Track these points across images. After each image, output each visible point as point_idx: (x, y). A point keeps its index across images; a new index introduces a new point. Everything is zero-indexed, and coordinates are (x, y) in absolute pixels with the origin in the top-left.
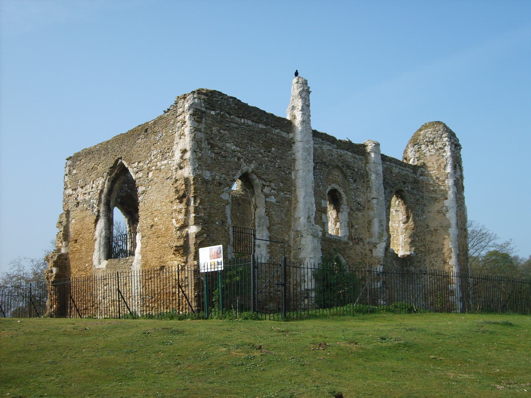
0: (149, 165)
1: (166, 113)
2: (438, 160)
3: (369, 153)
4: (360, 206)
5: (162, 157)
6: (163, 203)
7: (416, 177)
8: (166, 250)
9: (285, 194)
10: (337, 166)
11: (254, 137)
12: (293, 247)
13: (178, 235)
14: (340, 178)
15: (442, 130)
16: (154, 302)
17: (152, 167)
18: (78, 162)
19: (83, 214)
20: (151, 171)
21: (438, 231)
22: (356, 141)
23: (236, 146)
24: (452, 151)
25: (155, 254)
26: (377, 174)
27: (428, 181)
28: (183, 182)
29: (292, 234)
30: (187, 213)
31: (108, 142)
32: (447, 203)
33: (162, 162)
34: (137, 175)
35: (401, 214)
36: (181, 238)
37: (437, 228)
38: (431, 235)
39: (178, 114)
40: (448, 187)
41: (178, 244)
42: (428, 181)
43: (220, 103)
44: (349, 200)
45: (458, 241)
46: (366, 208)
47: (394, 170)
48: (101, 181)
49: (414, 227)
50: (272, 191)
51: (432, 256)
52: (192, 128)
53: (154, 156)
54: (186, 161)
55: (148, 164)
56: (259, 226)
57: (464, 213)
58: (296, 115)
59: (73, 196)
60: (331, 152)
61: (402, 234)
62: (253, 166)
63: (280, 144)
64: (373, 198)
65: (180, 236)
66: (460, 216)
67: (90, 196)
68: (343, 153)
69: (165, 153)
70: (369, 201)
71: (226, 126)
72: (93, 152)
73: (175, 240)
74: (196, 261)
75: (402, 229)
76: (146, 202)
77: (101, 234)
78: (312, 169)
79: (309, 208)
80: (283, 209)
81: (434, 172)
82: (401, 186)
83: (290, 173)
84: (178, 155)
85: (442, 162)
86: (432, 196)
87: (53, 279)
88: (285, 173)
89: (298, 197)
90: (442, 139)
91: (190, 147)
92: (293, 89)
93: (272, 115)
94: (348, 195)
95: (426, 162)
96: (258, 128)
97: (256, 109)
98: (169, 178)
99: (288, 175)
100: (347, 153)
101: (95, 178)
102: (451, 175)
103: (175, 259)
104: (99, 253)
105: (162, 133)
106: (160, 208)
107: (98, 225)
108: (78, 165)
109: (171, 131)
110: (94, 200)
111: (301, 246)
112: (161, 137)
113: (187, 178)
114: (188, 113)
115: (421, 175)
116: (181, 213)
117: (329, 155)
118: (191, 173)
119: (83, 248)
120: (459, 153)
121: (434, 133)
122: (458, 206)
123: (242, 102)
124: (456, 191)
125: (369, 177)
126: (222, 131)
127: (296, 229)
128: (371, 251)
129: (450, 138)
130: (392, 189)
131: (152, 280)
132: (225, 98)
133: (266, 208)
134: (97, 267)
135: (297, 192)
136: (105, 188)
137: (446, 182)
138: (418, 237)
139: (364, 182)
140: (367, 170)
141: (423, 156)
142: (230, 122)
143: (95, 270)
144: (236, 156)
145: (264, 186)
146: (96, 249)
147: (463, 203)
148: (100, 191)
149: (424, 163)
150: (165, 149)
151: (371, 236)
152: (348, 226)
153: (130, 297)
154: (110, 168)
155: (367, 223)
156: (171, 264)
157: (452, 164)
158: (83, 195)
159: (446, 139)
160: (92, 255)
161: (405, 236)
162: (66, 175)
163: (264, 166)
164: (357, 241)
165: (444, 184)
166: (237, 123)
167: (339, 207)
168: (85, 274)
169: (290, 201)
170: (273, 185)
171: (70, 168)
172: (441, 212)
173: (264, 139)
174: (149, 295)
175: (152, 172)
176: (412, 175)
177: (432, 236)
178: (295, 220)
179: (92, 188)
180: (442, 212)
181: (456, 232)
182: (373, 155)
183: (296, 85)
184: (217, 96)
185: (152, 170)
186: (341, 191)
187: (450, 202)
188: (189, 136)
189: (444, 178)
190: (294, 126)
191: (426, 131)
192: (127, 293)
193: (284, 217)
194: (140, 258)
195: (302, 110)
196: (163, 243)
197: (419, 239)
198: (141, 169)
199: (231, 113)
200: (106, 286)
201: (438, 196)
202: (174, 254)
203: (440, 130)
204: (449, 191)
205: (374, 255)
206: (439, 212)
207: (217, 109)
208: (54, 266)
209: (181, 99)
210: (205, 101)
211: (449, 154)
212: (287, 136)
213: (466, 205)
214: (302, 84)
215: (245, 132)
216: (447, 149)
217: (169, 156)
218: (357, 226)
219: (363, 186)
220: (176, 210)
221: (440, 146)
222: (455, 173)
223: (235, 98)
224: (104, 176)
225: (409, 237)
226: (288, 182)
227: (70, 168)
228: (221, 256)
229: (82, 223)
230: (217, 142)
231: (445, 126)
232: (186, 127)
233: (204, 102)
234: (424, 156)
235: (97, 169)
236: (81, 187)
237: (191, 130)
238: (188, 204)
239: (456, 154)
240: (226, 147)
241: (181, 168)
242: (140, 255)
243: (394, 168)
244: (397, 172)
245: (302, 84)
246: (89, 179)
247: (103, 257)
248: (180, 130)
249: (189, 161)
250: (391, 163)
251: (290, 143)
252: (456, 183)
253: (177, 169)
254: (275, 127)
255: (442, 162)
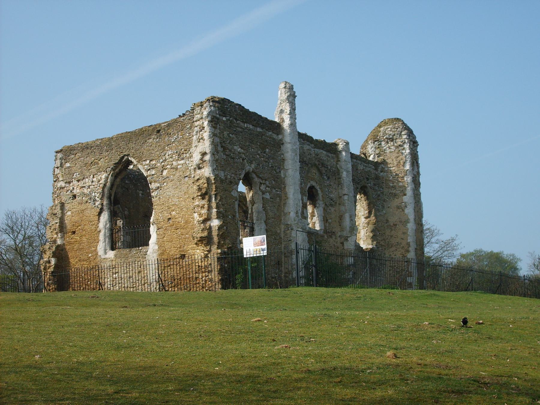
0: (163, 164)
1: (182, 117)
2: (398, 157)
3: (340, 152)
4: (333, 201)
5: (178, 157)
6: (181, 199)
7: (377, 173)
8: (187, 240)
9: (276, 191)
10: (315, 165)
11: (254, 139)
12: (283, 239)
13: (202, 227)
14: (317, 176)
15: (401, 127)
16: (175, 286)
17: (167, 166)
18: (73, 156)
19: (83, 207)
20: (166, 169)
21: (398, 226)
22: (329, 140)
23: (241, 148)
24: (411, 149)
25: (174, 244)
26: (348, 172)
27: (387, 177)
28: (205, 181)
29: (283, 227)
30: (210, 208)
31: (112, 138)
32: (406, 199)
33: (179, 162)
34: (148, 172)
35: (363, 209)
36: (205, 230)
37: (396, 223)
38: (390, 230)
39: (195, 119)
40: (407, 183)
41: (203, 235)
42: (387, 177)
43: (230, 110)
44: (324, 196)
45: (415, 236)
46: (338, 203)
47: (360, 167)
48: (104, 176)
49: (376, 221)
50: (267, 188)
51: (391, 249)
52: (211, 133)
53: (168, 155)
54: (205, 163)
55: (162, 162)
56: (257, 220)
57: (420, 209)
58: (285, 118)
59: (66, 188)
60: (310, 152)
61: (364, 229)
62: (253, 166)
63: (272, 146)
64: (344, 195)
65: (204, 228)
66: (418, 211)
67: (89, 190)
68: (319, 152)
69: (182, 154)
70: (341, 197)
71: (234, 131)
72: (91, 147)
73: (199, 231)
74: (220, 250)
75: (364, 224)
76: (162, 197)
77: (105, 226)
78: (298, 168)
79: (297, 204)
80: (275, 204)
81: (394, 168)
82: (365, 183)
83: (280, 172)
84: (196, 158)
85: (402, 159)
86: (392, 192)
87: (52, 269)
88: (276, 172)
89: (288, 194)
90: (402, 136)
91: (210, 150)
92: (281, 94)
93: (266, 119)
94: (323, 191)
95: (386, 159)
96: (257, 131)
97: (255, 114)
98: (187, 176)
99: (278, 174)
100: (322, 152)
101: (96, 173)
102: (410, 172)
103: (197, 248)
104: (104, 244)
105: (178, 135)
106: (178, 203)
107: (102, 218)
108: (72, 159)
109: (188, 135)
110: (96, 194)
111: (291, 238)
112: (176, 139)
113: (208, 178)
114: (207, 120)
115: (381, 172)
116: (203, 208)
117: (309, 155)
118: (211, 173)
119: (84, 239)
120: (416, 149)
121: (393, 130)
122: (416, 202)
123: (245, 109)
124: (414, 188)
125: (341, 174)
126: (231, 135)
127: (286, 223)
128: (342, 243)
129: (409, 136)
130: (358, 186)
131: (171, 267)
132: (233, 105)
133: (263, 204)
134: (103, 257)
135: (287, 189)
136: (108, 182)
137: (405, 179)
138: (379, 231)
139: (335, 179)
140: (339, 168)
141: (383, 152)
142: (237, 127)
143: (100, 260)
144: (241, 157)
145: (261, 184)
146: (102, 240)
147: (420, 199)
148: (103, 186)
149: (384, 159)
150: (181, 150)
151: (342, 230)
152: (324, 220)
153: (145, 283)
154: (115, 164)
155: (338, 218)
156: (193, 252)
157: (410, 161)
158: (80, 188)
159: (405, 137)
160: (97, 246)
161: (367, 230)
162: (57, 168)
163: (261, 165)
164: (330, 234)
165: (403, 181)
166: (241, 128)
167: (315, 202)
168: (87, 263)
169: (280, 197)
170: (267, 183)
171: (61, 161)
172: (400, 207)
173: (261, 141)
174: (168, 281)
175: (167, 170)
176: (374, 171)
177: (392, 230)
178: (285, 214)
179: (92, 182)
180: (401, 208)
181: (414, 227)
182: (344, 153)
183: (283, 90)
184: (227, 103)
185: (166, 169)
186: (318, 188)
187: (408, 198)
188: (209, 140)
189: (403, 175)
190: (283, 128)
191: (386, 128)
192: (141, 280)
193: (276, 212)
194: (157, 247)
195: (290, 114)
196: (183, 234)
197: (379, 234)
198: (154, 167)
199: (238, 119)
200: (115, 274)
201: (397, 192)
202: (196, 244)
203: (399, 128)
204: (408, 187)
205: (346, 247)
206: (398, 207)
207: (227, 115)
208: (53, 257)
209: (198, 106)
210: (219, 109)
211: (408, 151)
212: (277, 138)
213: (422, 201)
214: (289, 89)
215: (247, 135)
216: (407, 146)
217: (186, 156)
218: (330, 221)
219: (334, 183)
220: (198, 206)
221: (399, 143)
222: (413, 170)
223: (240, 105)
224: (107, 171)
225: (372, 232)
226: (279, 180)
227: (61, 161)
228: (265, 244)
229: (81, 215)
230: (227, 145)
231: (403, 123)
232: (205, 132)
233: (218, 110)
234: (384, 153)
235: (98, 164)
236: (77, 181)
237: (210, 135)
238: (210, 201)
239: (414, 151)
240: (234, 150)
241: (200, 168)
242: (157, 245)
243: (359, 166)
244: (362, 169)
245: (289, 89)
246: (88, 173)
247: (108, 247)
248: (198, 134)
249: (209, 163)
250: (357, 160)
251: (279, 144)
252: (414, 180)
253: (195, 169)
254: (269, 130)
255: (402, 159)
